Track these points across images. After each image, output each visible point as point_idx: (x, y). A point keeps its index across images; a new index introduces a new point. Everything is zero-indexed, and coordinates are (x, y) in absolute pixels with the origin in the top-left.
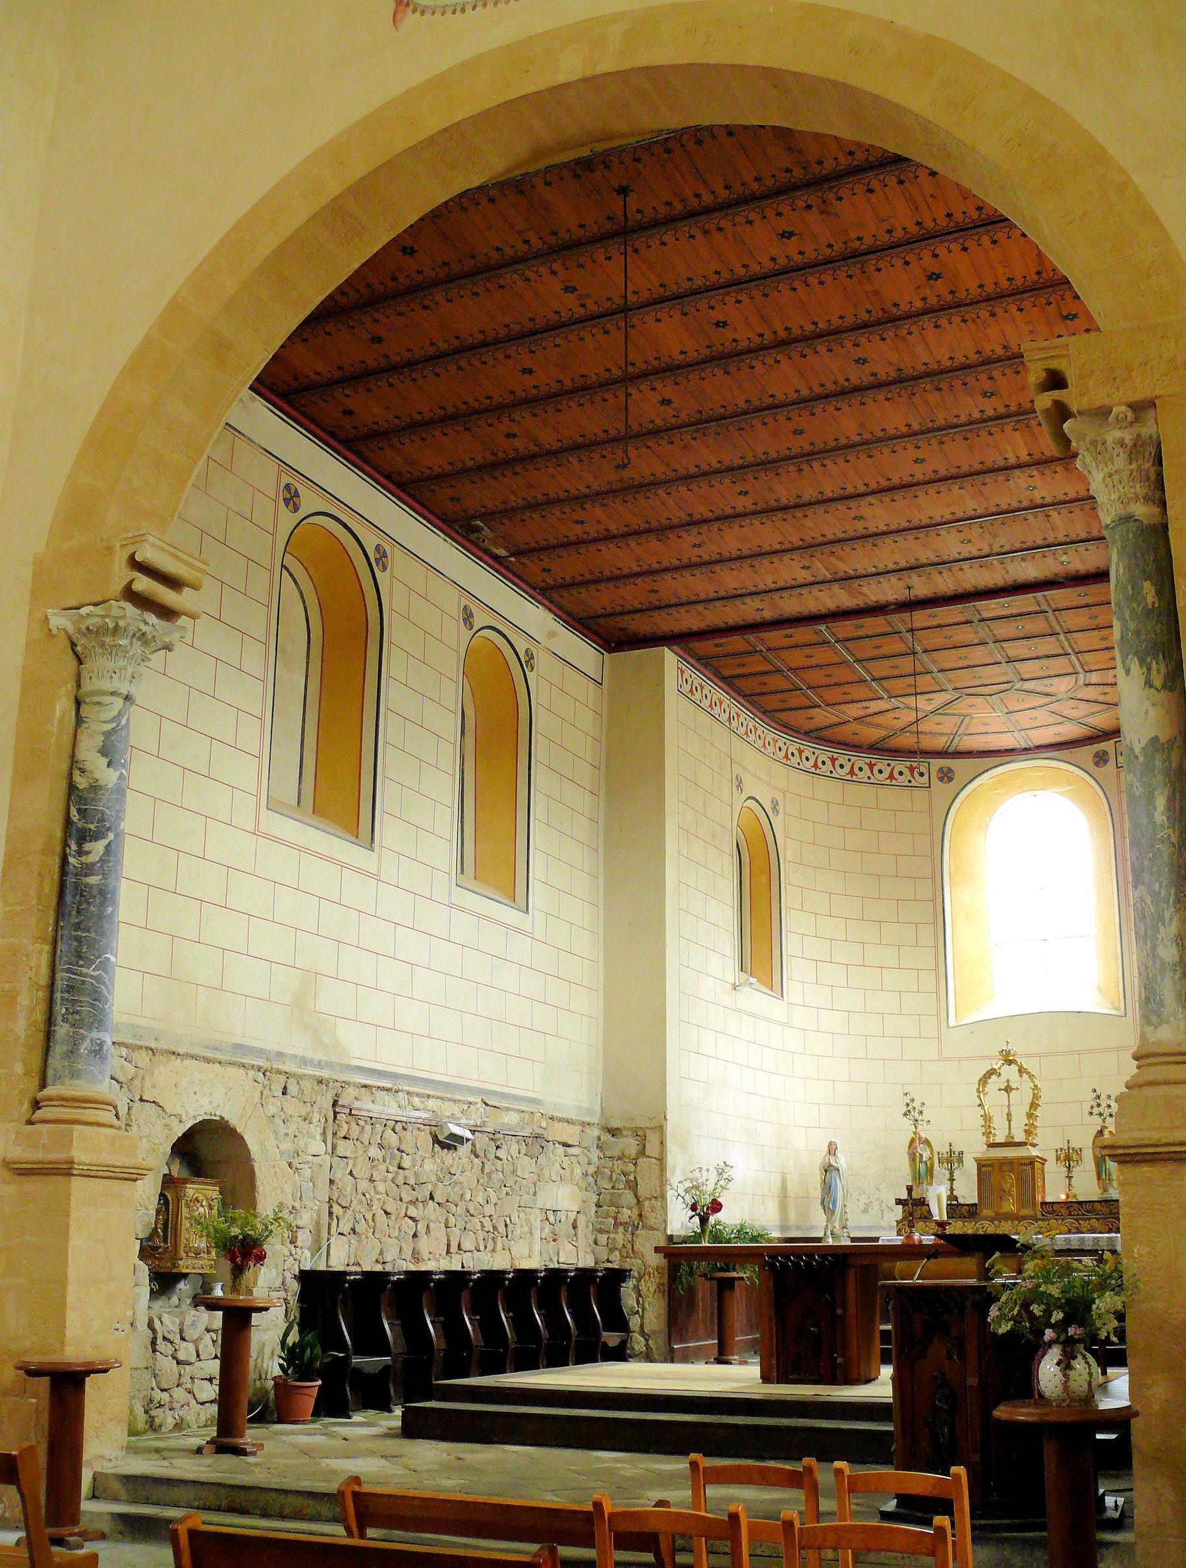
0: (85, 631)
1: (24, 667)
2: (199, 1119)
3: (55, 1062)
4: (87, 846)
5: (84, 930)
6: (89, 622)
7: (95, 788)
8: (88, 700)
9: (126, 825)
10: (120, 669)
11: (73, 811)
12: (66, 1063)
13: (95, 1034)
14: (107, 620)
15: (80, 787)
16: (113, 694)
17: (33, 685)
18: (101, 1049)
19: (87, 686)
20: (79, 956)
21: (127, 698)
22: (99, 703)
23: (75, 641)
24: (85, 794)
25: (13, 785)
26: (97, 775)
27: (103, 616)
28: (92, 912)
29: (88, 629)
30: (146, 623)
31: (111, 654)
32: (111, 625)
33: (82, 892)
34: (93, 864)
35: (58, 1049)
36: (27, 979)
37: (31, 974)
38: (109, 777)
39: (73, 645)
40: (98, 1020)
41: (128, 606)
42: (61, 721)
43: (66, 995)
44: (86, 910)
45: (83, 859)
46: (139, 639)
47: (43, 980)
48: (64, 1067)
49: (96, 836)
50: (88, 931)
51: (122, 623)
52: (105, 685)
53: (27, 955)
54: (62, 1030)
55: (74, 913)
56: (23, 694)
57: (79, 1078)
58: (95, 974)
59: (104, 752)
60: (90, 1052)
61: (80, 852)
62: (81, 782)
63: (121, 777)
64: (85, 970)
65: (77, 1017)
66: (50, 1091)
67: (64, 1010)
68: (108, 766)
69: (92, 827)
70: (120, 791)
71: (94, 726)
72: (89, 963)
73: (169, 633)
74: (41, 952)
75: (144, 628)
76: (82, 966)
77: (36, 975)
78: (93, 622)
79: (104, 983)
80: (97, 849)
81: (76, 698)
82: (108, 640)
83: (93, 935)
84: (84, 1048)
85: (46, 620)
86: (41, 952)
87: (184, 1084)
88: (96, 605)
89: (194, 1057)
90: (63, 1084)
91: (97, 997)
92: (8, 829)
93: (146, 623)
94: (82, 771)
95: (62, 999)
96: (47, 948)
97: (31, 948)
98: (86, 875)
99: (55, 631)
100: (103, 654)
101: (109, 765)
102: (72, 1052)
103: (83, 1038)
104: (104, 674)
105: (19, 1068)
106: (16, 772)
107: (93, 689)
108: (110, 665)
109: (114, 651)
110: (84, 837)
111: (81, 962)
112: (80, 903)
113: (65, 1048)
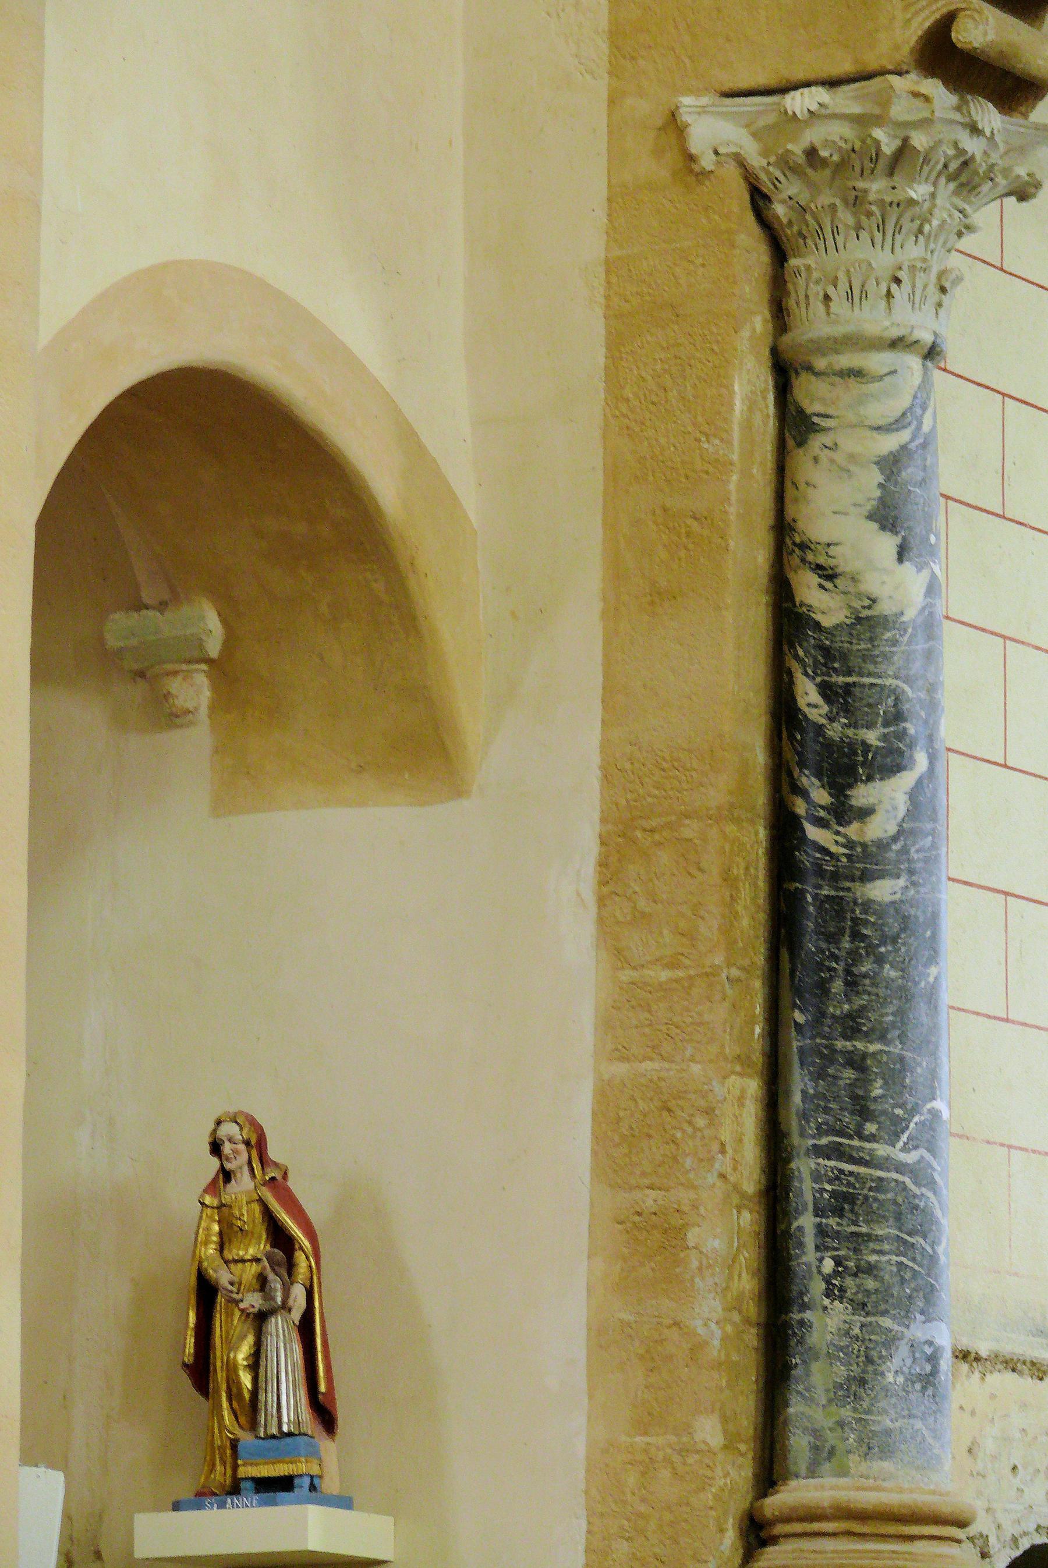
0: (801, 159)
1: (610, 266)
2: (1025, 1544)
3: (808, 1409)
4: (862, 795)
5: (867, 1036)
6: (813, 135)
7: (868, 623)
8: (820, 364)
9: (950, 730)
10: (912, 268)
11: (808, 694)
12: (846, 1413)
13: (918, 1331)
14: (878, 133)
15: (826, 622)
16: (896, 344)
17: (640, 318)
18: (934, 1373)
19: (813, 323)
20: (863, 1109)
21: (932, 353)
22: (857, 373)
23: (767, 187)
24: (841, 642)
25: (612, 614)
26: (871, 584)
27: (861, 121)
28: (889, 983)
29: (811, 153)
30: (974, 130)
31: (881, 227)
32: (889, 147)
33: (846, 920)
34: (882, 845)
35: (816, 1380)
36: (712, 1178)
37: (723, 1163)
38: (899, 588)
39: (759, 199)
40: (919, 1292)
41: (934, 87)
42: (747, 426)
43: (832, 1222)
44: (874, 978)
45: (852, 830)
46: (951, 178)
47: (750, 1176)
48: (841, 1424)
49: (889, 762)
50: (883, 1038)
51: (920, 141)
52: (872, 319)
53: (709, 1112)
54: (825, 1322)
55: (837, 986)
56: (615, 344)
57: (887, 1452)
58: (910, 1158)
59: (887, 516)
60: (911, 1379)
61: (842, 812)
62: (826, 607)
63: (932, 589)
64: (881, 1150)
65: (870, 1284)
66: (791, 1495)
67: (828, 1265)
68: (901, 558)
69: (872, 737)
70: (929, 626)
71: (849, 443)
72: (895, 1130)
73: (1021, 151)
74: (741, 1100)
75: (973, 146)
76: (872, 1138)
77: (736, 1164)
78: (832, 136)
79: (932, 1184)
80: (887, 799)
81: (775, 352)
82: (876, 187)
83: (896, 1049)
84: (894, 1371)
85: (674, 126)
86: (741, 1100)
87: (989, 1445)
88: (832, 83)
89: (1011, 1365)
90: (843, 1472)
91: (913, 1221)
92: (606, 745)
93: (974, 130)
94: (828, 574)
95: (821, 1231)
96: (754, 1086)
97: (719, 1090)
98: (865, 877)
99: (707, 162)
100: (859, 228)
101: (902, 554)
102: (857, 1386)
103: (891, 1341)
104: (852, 287)
105: (709, 1431)
106: (616, 574)
107: (838, 330)
108: (883, 260)
109: (889, 219)
110: (845, 767)
111: (871, 1128)
112: (855, 957)
113: (841, 1371)
